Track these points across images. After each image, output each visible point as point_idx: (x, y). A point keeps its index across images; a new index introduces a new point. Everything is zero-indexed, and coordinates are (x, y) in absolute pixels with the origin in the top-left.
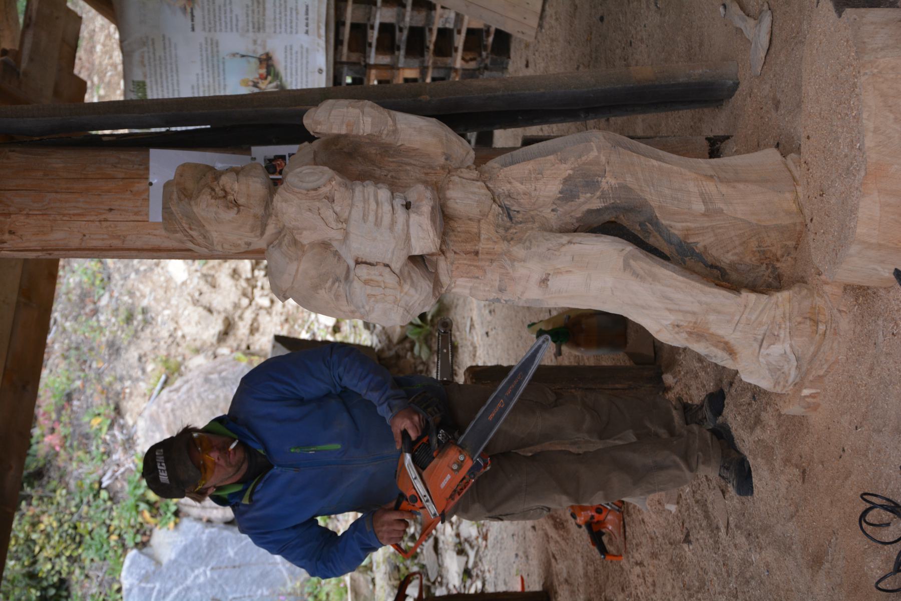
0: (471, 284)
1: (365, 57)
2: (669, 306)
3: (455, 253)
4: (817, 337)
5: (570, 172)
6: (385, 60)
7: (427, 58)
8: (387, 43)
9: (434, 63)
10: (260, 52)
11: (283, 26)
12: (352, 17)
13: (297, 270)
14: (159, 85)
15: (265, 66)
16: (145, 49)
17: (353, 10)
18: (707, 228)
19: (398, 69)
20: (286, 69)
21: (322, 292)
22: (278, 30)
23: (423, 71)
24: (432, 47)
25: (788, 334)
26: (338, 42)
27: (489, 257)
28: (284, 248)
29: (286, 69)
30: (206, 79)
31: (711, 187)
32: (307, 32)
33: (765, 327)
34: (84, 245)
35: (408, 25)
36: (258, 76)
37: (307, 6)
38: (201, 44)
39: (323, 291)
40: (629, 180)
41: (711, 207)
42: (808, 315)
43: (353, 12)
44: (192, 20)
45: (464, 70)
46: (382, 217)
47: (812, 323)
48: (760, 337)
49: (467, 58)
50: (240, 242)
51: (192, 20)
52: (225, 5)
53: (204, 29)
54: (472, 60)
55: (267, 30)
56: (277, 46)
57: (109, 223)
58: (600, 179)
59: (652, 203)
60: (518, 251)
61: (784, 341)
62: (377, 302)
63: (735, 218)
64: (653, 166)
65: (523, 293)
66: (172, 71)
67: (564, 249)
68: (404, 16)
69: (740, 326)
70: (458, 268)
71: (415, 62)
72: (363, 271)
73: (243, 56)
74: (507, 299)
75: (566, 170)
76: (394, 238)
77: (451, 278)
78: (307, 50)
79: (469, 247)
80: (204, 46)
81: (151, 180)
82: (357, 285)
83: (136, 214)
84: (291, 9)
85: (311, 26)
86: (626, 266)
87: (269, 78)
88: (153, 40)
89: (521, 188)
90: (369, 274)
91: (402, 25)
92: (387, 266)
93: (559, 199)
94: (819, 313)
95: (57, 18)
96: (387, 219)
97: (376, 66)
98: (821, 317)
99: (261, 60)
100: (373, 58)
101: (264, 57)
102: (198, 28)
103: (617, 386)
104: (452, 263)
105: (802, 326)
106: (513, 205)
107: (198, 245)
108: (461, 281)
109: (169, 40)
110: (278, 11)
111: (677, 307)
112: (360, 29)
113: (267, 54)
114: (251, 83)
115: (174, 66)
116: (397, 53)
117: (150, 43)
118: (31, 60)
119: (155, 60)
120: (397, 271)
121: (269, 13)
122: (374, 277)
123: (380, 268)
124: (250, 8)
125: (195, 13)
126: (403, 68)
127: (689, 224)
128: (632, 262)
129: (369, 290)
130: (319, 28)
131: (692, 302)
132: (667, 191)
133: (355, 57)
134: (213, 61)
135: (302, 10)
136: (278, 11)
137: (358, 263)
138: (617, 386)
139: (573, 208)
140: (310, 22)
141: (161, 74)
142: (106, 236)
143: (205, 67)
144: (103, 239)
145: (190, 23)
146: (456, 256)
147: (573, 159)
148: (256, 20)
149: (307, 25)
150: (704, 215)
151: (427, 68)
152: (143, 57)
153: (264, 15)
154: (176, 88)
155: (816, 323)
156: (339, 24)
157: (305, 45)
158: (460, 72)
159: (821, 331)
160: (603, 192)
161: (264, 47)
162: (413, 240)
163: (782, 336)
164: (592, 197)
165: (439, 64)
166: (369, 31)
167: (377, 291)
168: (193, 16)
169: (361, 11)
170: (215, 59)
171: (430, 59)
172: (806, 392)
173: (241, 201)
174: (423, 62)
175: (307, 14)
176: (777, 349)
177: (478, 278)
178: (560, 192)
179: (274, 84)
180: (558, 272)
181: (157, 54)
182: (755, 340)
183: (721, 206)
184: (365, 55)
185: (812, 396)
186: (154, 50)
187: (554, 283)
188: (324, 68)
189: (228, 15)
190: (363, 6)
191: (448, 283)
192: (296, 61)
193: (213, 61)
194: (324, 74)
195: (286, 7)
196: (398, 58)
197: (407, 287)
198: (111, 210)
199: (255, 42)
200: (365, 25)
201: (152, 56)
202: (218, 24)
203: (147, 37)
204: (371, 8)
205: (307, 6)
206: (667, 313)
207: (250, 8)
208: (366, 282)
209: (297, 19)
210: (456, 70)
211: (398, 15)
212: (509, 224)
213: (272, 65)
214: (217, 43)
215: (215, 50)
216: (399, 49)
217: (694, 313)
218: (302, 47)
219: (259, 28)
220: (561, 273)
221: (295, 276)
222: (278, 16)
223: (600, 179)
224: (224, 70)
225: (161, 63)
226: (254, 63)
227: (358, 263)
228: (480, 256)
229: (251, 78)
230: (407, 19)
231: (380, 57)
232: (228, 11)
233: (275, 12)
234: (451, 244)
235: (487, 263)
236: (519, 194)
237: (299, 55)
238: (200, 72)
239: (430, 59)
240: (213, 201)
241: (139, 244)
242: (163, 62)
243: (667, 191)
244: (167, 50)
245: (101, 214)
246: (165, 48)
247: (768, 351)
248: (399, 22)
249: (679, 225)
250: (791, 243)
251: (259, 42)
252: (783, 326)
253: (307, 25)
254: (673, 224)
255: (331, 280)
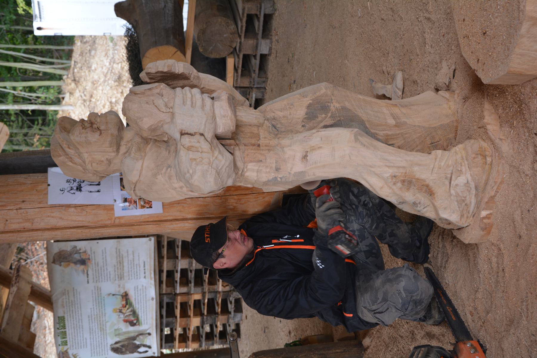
0: (256, 168)
1: (174, 289)
2: (387, 164)
3: (245, 145)
4: (487, 167)
5: (311, 101)
6: (184, 290)
7: (205, 287)
8: (185, 281)
9: (209, 289)
10: (122, 291)
11: (133, 275)
12: (167, 267)
13: (142, 167)
14: (72, 318)
15: (125, 299)
16: (64, 297)
17: (167, 262)
18: (399, 134)
19: (191, 294)
20: (135, 300)
21: (160, 177)
22: (131, 278)
23: (204, 294)
24: (207, 280)
25: (467, 168)
26: (161, 282)
27: (267, 148)
28: (133, 155)
29: (135, 300)
30: (95, 311)
31: (396, 110)
32: (145, 277)
33: (451, 168)
34: (7, 229)
35: (194, 268)
36: (121, 306)
37: (144, 262)
38: (92, 291)
39: (160, 176)
40: (347, 105)
41: (398, 121)
42: (479, 152)
43: (167, 264)
44: (88, 277)
45: (223, 292)
46: (196, 102)
47: (482, 157)
48: (449, 176)
49: (225, 285)
50: (103, 159)
51: (88, 277)
52: (104, 266)
53: (94, 281)
54: (226, 286)
55: (125, 278)
56: (130, 287)
57: (23, 210)
58: (329, 104)
59: (363, 118)
60: (285, 142)
61: (465, 174)
62: (197, 164)
63: (415, 126)
64: (360, 99)
65: (292, 168)
66: (78, 308)
67: (314, 135)
68: (192, 263)
69: (436, 170)
70: (248, 155)
71: (199, 289)
72: (186, 140)
73: (114, 295)
74: (281, 176)
75: (307, 101)
76: (205, 114)
77: (244, 163)
78: (146, 287)
79: (253, 141)
80: (94, 291)
81: (49, 183)
82: (183, 153)
83: (40, 203)
84: (137, 265)
85: (147, 273)
86: (356, 140)
87: (127, 306)
88: (68, 291)
89: (281, 114)
90: (190, 142)
91: (191, 269)
92: (202, 135)
93: (305, 118)
94: (485, 151)
95: (22, 305)
96: (199, 103)
97: (181, 294)
98: (487, 153)
99: (123, 296)
100: (179, 289)
101: (124, 294)
102: (91, 281)
103: (337, 351)
104: (243, 152)
105: (476, 159)
106: (277, 124)
107: (75, 164)
108: (250, 166)
109: (76, 290)
110: (130, 267)
111: (392, 165)
112: (170, 274)
113: (126, 292)
114: (118, 311)
115: (79, 305)
116: (190, 285)
117: (67, 292)
118: (7, 324)
119: (69, 303)
120: (209, 140)
121: (126, 269)
122: (194, 144)
123: (197, 136)
124: (116, 267)
125: (89, 273)
126: (193, 294)
127: (387, 132)
128: (359, 137)
129: (192, 155)
130: (151, 274)
131: (401, 161)
132: (371, 113)
133: (169, 290)
134: (98, 299)
135: (142, 265)
136: (130, 267)
137: (182, 134)
138: (337, 351)
139: (315, 125)
140: (146, 271)
141: (72, 311)
142: (21, 220)
143: (95, 303)
144: (19, 223)
145: (86, 279)
146: (246, 147)
147: (311, 95)
148: (119, 273)
149: (145, 273)
150: (395, 126)
151: (205, 293)
152: (63, 302)
153: (123, 270)
154: (80, 318)
155: (485, 157)
156: (161, 271)
157: (145, 285)
158: (221, 294)
159: (488, 162)
160: (332, 112)
161: (124, 288)
162: (218, 119)
163: (464, 170)
164: (326, 117)
165: (211, 290)
166: (176, 274)
167: (197, 155)
168: (88, 275)
169: (171, 262)
170: (100, 298)
171: (206, 287)
172: (484, 213)
173: (102, 127)
174: (203, 289)
175: (144, 266)
176: (461, 180)
177: (261, 161)
178: (306, 114)
179: (130, 310)
180: (313, 149)
181: (70, 299)
182: (446, 178)
183: (405, 120)
184: (174, 287)
185: (488, 217)
186: (69, 296)
187: (312, 157)
188: (154, 297)
189: (105, 272)
190: (172, 260)
191: (242, 167)
192: (140, 295)
193: (98, 299)
194: (155, 300)
195: (134, 264)
196: (191, 288)
197: (216, 153)
198: (23, 201)
199: (119, 286)
200: (173, 271)
201: (67, 300)
202: (100, 278)
203: (65, 290)
204: (176, 261)
205: (144, 262)
206: (387, 169)
207: (116, 267)
208: (189, 149)
209: (140, 270)
210: (219, 292)
211: (189, 263)
212: (276, 133)
213: (128, 299)
214: (100, 289)
215: (99, 293)
216: (191, 283)
217: (404, 167)
218: (143, 286)
219: (121, 277)
220: (315, 149)
221: (141, 170)
222: (130, 270)
223: (329, 104)
224: (104, 304)
225: (72, 304)
226: (119, 298)
227: (182, 134)
228: (261, 148)
229: (118, 308)
230: (194, 265)
231: (182, 288)
232: (105, 269)
233: (128, 267)
234: (242, 139)
235: (266, 152)
236: (280, 117)
237: (142, 291)
238: (92, 307)
239: (206, 287)
240: (84, 130)
241: (42, 225)
242: (73, 303)
243: (371, 113)
244: (76, 296)
245: (17, 204)
246: (74, 296)
247: (456, 182)
248: (190, 267)
249: (381, 133)
250: (452, 136)
251: (121, 286)
252: (463, 164)
253: (145, 273)
254: (377, 132)
255: (165, 168)
